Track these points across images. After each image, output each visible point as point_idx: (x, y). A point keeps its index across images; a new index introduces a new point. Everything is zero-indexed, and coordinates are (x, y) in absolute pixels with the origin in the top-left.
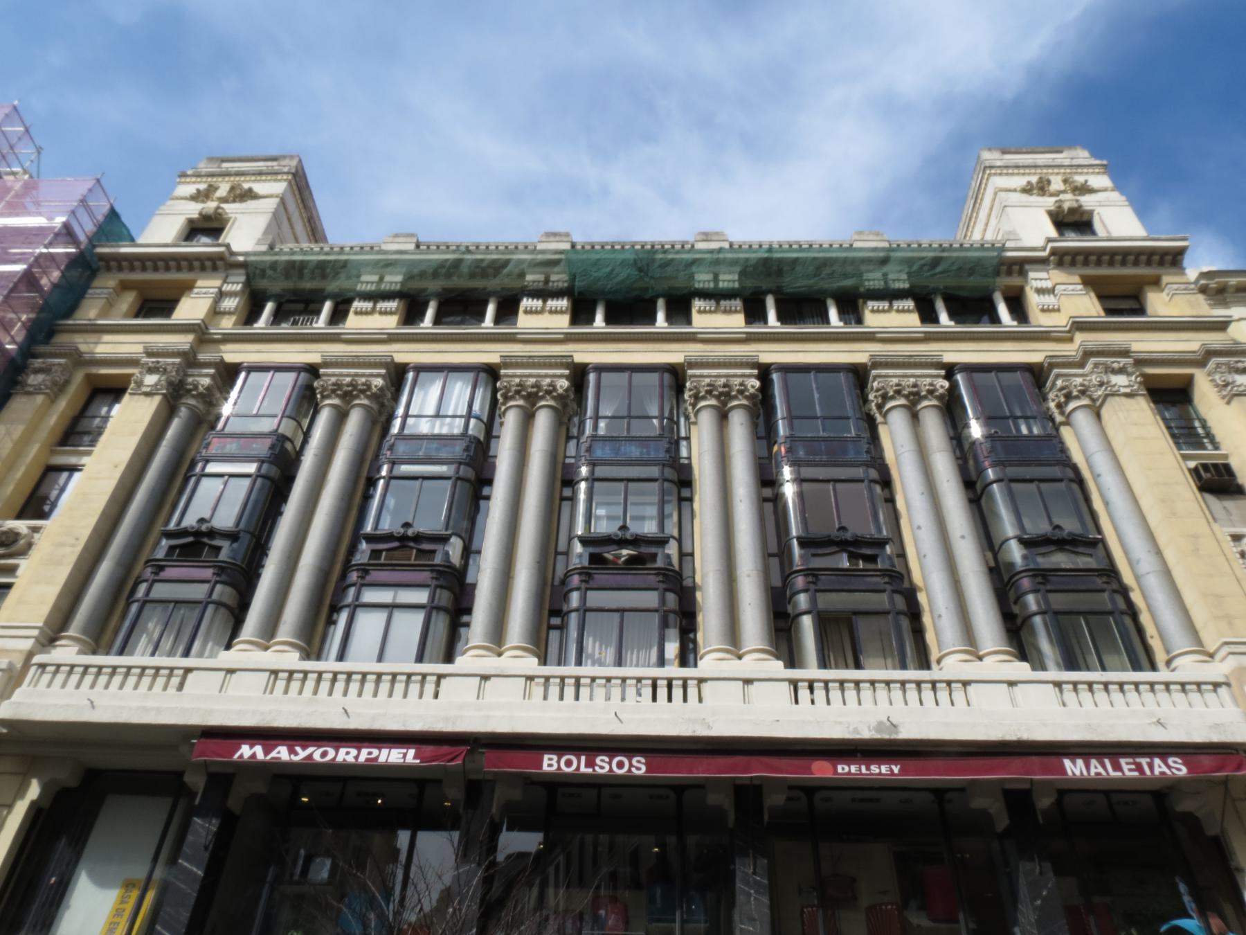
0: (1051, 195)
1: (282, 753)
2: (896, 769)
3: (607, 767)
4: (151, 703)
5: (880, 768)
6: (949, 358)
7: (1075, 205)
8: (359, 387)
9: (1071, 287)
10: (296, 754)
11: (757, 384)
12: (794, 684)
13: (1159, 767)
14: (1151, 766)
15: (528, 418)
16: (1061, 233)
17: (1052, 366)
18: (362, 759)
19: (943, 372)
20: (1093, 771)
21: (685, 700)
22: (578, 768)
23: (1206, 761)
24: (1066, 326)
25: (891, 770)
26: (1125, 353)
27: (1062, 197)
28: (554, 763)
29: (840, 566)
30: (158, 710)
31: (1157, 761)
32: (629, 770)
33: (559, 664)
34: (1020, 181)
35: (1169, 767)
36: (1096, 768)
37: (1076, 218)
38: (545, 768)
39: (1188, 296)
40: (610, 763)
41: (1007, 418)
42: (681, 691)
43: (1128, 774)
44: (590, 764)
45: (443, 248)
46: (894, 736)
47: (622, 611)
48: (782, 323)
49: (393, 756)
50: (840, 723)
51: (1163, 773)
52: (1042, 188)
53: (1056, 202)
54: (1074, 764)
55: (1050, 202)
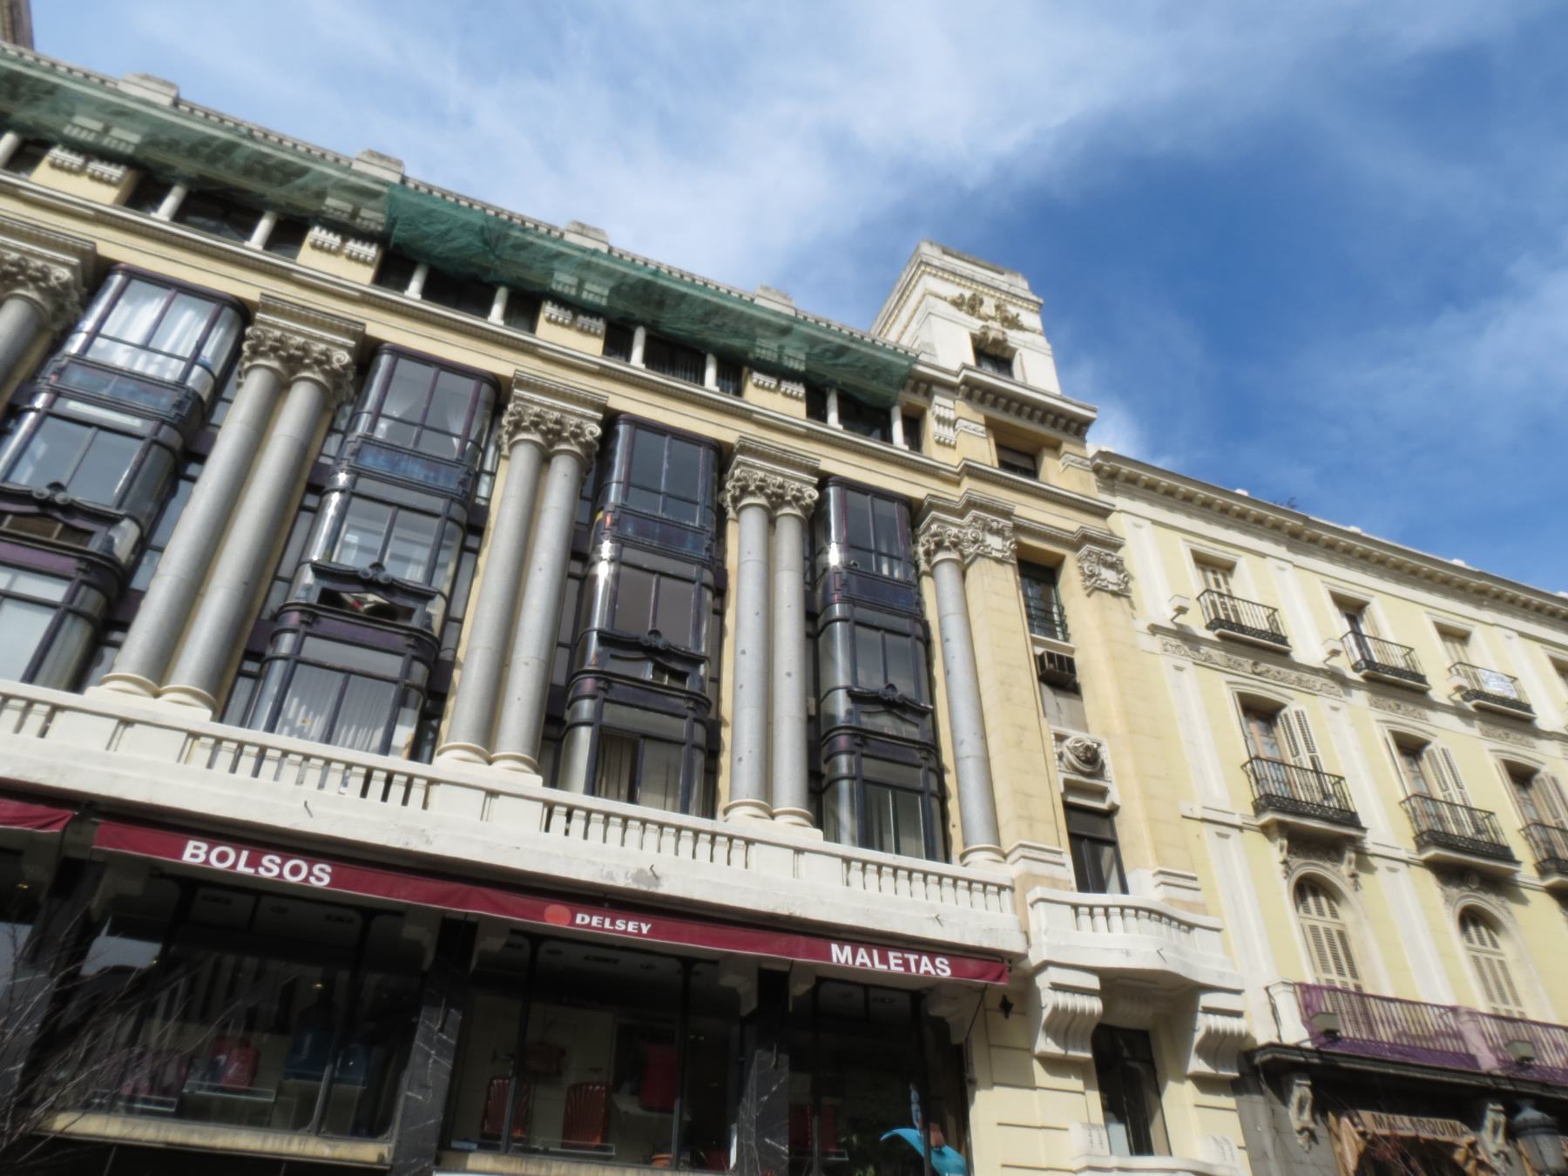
0: (980, 318)
2: (645, 929)
5: (627, 925)
6: (827, 465)
7: (1000, 337)
8: (30, 272)
9: (973, 426)
11: (598, 431)
12: (550, 807)
14: (918, 963)
15: (280, 389)
17: (932, 506)
19: (816, 480)
20: (859, 960)
22: (234, 865)
23: (972, 965)
25: (640, 929)
26: (1007, 514)
27: (990, 323)
31: (925, 959)
32: (306, 880)
33: (242, 724)
34: (953, 291)
35: (935, 967)
37: (998, 352)
39: (1083, 472)
40: (281, 866)
41: (870, 551)
43: (893, 968)
45: (214, 119)
46: (652, 889)
47: (348, 672)
49: (928, 967)
50: (594, 863)
51: (927, 972)
53: (983, 327)
55: (976, 325)
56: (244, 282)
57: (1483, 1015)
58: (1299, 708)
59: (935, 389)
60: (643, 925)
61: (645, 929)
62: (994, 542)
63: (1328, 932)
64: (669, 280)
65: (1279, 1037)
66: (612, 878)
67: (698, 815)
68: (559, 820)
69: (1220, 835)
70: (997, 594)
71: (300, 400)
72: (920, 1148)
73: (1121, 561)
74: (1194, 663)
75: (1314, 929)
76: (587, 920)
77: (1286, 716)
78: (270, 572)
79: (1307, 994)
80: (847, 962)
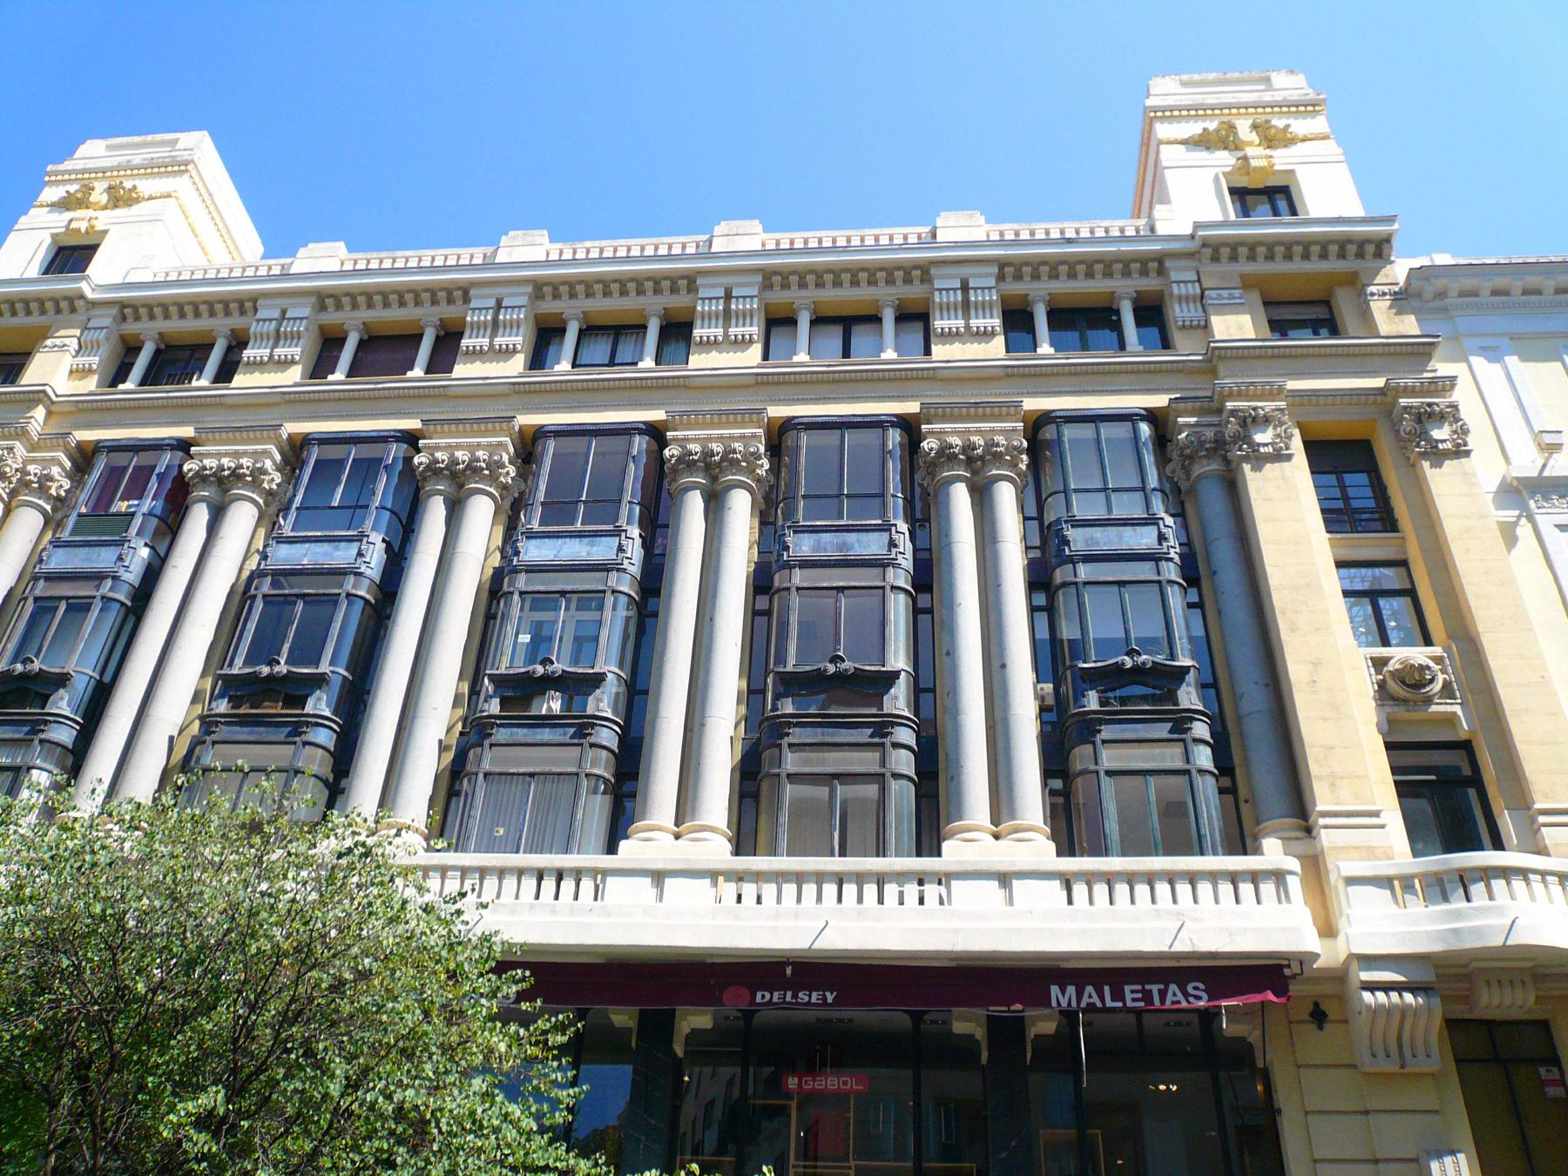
5: (810, 996)
9: (1225, 293)
14: (1163, 994)
15: (715, 503)
16: (1245, 211)
24: (57, 396)
25: (825, 998)
31: (1173, 988)
35: (1186, 995)
43: (1129, 1004)
52: (1223, 139)
54: (1063, 992)
59: (1168, 264)
60: (828, 994)
61: (830, 997)
64: (575, 265)
65: (1331, 1022)
67: (1224, 854)
68: (1080, 889)
71: (740, 507)
73: (1455, 407)
76: (768, 995)
78: (1223, 685)
80: (1069, 1004)
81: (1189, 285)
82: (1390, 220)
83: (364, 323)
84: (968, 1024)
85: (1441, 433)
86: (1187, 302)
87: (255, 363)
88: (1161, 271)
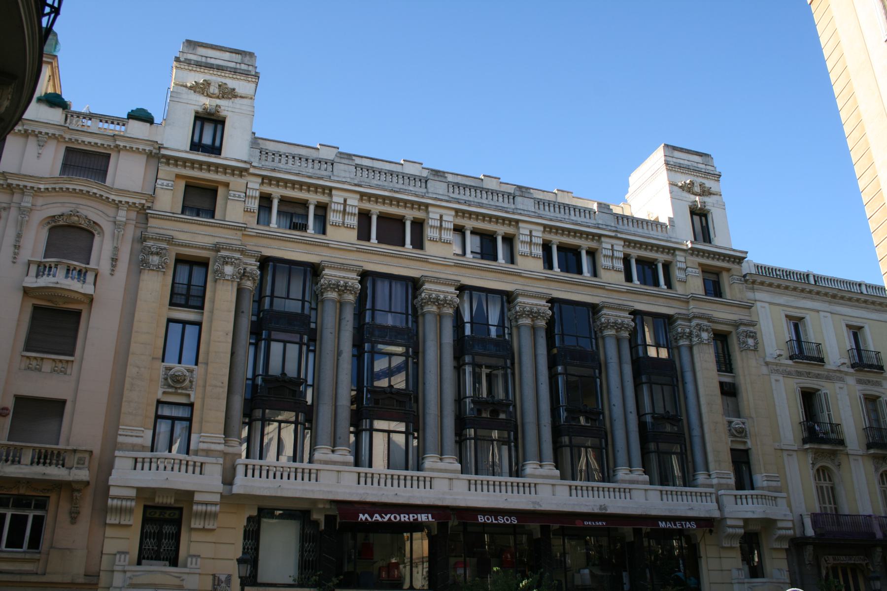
1: (377, 517)
3: (483, 520)
4: (307, 488)
9: (694, 270)
10: (384, 518)
12: (661, 491)
13: (688, 525)
14: (685, 524)
18: (411, 519)
20: (668, 526)
21: (476, 490)
22: (492, 521)
28: (482, 518)
29: (666, 430)
30: (312, 491)
31: (688, 523)
36: (669, 525)
37: (702, 212)
38: (480, 521)
39: (740, 285)
42: (474, 486)
44: (496, 519)
48: (561, 271)
51: (689, 527)
56: (256, 89)
57: (883, 517)
58: (825, 391)
62: (705, 335)
63: (827, 487)
66: (541, 506)
69: (788, 455)
70: (706, 361)
72: (683, 578)
74: (715, 236)
75: (822, 487)
77: (820, 394)
79: (815, 518)
81: (339, 205)
82: (747, 253)
83: (317, 202)
84: (628, 530)
85: (751, 342)
86: (348, 215)
87: (537, 257)
88: (330, 195)
